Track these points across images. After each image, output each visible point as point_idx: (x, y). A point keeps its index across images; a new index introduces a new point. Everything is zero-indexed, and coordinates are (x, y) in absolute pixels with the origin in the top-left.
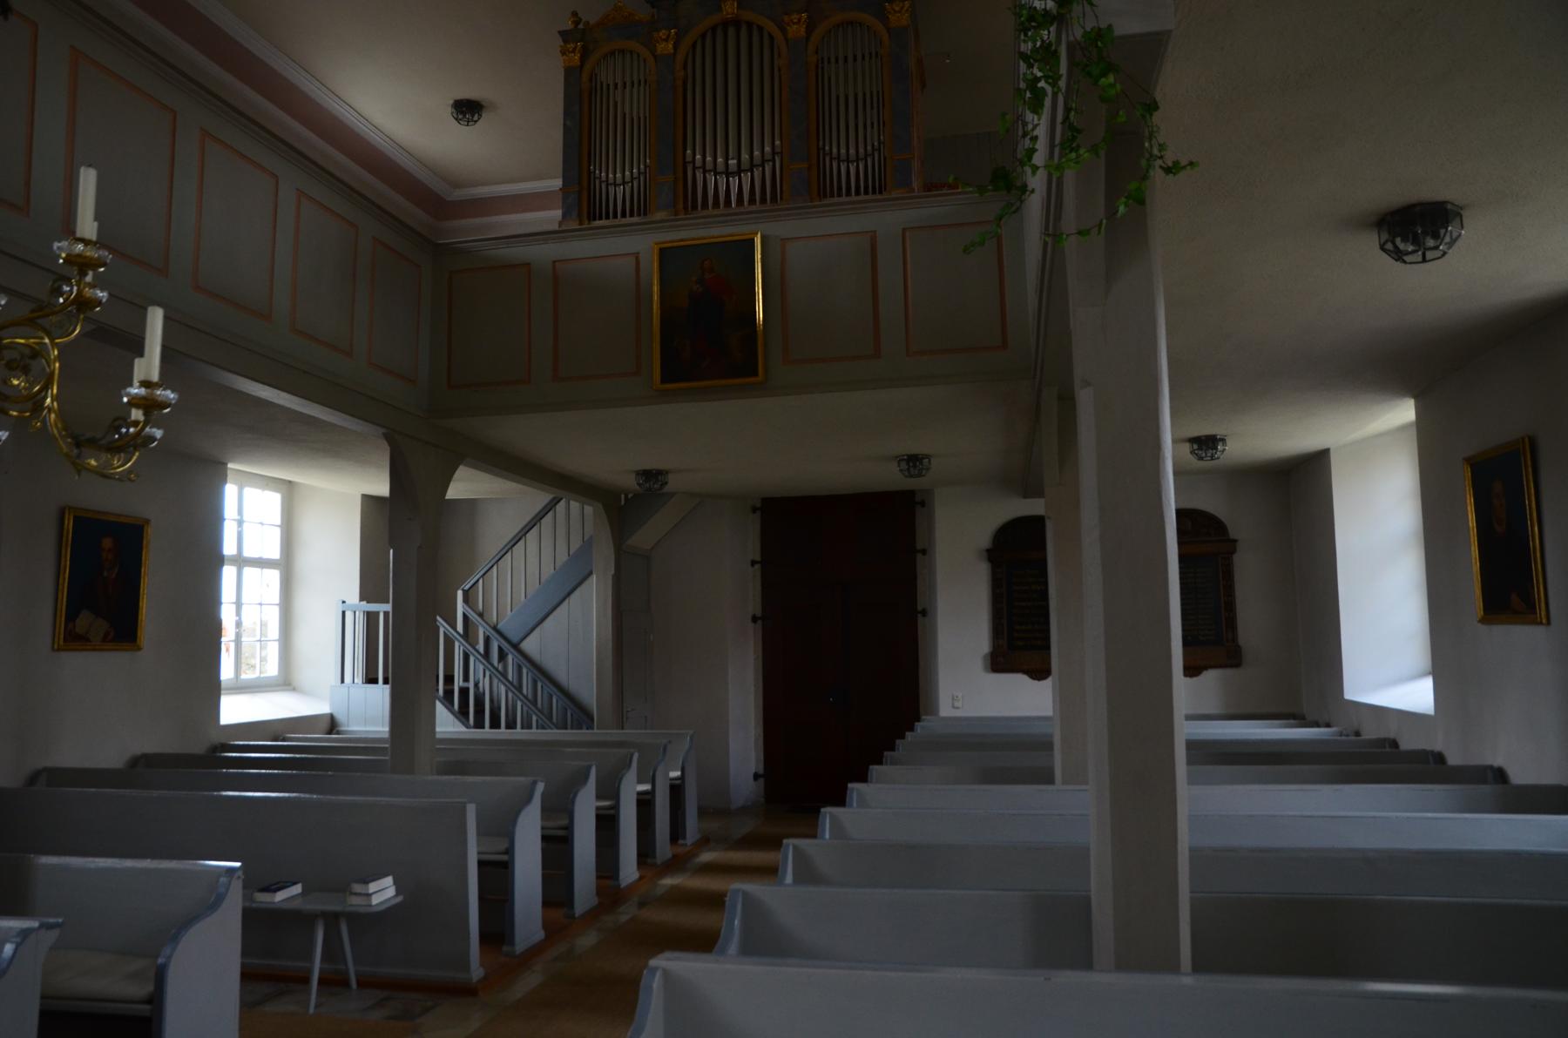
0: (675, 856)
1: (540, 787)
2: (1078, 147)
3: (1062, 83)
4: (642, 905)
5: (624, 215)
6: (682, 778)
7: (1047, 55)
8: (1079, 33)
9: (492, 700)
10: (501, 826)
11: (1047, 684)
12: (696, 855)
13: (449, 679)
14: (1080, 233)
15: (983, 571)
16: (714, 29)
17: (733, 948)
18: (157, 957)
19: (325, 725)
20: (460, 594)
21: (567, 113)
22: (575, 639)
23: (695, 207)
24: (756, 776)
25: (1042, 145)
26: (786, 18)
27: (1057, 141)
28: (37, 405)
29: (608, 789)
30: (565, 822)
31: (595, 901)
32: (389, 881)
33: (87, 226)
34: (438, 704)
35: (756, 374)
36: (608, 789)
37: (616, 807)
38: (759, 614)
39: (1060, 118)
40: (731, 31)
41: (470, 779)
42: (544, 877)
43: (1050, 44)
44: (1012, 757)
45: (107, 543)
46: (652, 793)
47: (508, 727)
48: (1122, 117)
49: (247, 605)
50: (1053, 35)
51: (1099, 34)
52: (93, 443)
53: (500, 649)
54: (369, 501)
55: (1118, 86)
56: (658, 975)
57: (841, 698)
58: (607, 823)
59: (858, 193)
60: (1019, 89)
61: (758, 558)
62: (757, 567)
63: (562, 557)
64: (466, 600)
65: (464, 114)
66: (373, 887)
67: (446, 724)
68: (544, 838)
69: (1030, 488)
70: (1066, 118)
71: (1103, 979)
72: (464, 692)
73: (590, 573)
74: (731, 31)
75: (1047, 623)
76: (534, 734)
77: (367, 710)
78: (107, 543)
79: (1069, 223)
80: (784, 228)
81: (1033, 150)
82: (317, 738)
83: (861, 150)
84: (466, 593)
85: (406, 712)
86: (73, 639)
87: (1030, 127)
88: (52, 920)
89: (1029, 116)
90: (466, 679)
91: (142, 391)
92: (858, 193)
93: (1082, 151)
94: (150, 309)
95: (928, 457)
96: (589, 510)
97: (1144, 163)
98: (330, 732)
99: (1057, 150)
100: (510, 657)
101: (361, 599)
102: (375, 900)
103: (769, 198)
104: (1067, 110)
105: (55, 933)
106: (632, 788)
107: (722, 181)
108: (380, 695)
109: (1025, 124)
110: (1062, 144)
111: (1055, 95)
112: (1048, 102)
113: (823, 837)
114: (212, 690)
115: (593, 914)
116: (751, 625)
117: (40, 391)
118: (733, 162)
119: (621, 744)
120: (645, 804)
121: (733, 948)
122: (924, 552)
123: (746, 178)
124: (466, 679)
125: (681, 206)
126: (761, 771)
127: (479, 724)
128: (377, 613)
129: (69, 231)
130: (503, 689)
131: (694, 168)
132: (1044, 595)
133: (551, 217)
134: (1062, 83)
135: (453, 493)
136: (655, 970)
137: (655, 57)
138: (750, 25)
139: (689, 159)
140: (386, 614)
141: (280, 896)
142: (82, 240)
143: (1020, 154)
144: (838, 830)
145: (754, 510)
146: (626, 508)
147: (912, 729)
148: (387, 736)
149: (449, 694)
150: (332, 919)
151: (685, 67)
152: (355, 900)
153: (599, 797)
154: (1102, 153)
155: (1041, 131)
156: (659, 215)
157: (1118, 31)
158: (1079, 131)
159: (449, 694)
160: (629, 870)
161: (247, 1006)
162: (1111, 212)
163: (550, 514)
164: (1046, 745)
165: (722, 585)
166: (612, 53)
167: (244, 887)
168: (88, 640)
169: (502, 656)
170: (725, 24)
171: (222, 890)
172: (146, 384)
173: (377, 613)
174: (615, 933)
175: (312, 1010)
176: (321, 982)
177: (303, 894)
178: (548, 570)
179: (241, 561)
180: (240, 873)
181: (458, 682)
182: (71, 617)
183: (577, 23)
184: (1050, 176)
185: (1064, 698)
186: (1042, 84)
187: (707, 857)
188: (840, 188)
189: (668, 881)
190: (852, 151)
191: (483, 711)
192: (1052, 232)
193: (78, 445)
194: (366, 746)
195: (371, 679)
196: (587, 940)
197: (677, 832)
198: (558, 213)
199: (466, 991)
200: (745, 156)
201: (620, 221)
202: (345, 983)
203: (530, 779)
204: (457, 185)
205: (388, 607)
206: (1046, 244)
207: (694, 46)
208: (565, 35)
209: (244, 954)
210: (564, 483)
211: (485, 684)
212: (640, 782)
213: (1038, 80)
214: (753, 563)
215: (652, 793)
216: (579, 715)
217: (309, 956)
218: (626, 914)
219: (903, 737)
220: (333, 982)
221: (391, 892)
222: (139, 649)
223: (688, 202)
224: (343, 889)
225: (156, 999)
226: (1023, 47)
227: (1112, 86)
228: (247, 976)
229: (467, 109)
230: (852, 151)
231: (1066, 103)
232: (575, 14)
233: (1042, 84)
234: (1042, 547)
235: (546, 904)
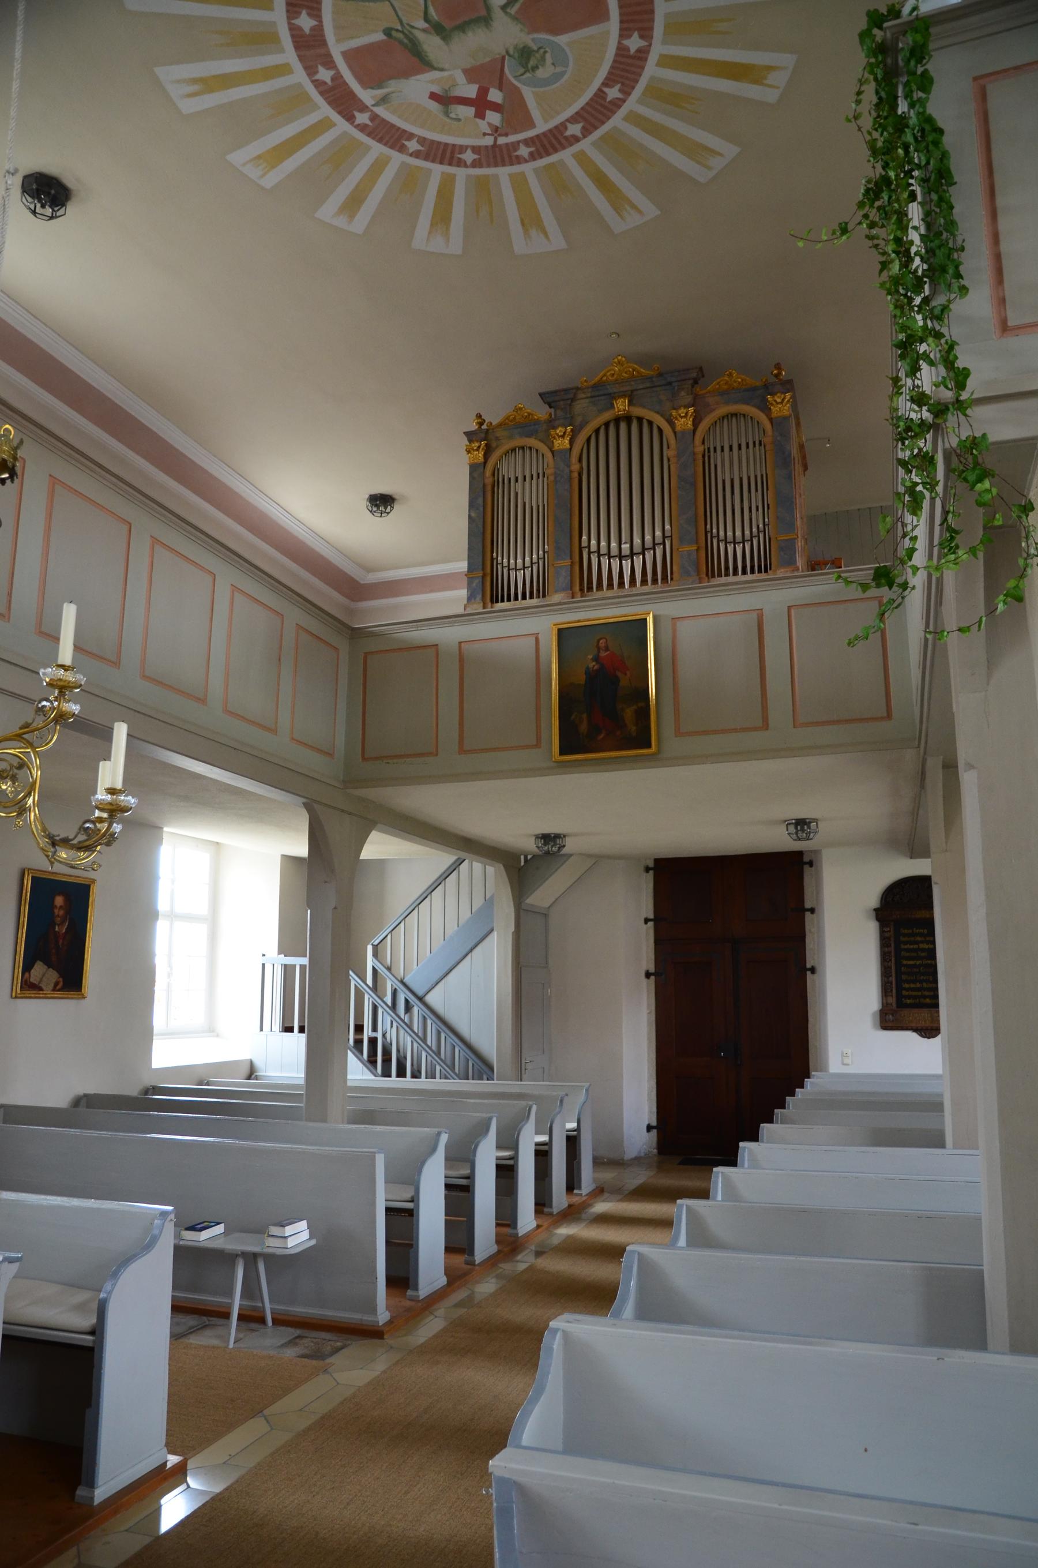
0: (570, 1206)
1: (444, 1138)
2: (957, 547)
3: (940, 488)
4: (539, 1254)
5: (524, 598)
6: (578, 1129)
7: (926, 461)
8: (954, 444)
9: (398, 1051)
10: (407, 1175)
11: (937, 1041)
12: (590, 1205)
13: (359, 1029)
14: (959, 630)
15: (872, 929)
16: (607, 425)
17: (629, 1310)
18: (100, 1291)
19: (245, 1071)
20: (370, 948)
21: (472, 505)
22: (476, 994)
23: (590, 588)
24: (649, 1128)
25: (921, 545)
26: (674, 413)
27: (936, 542)
28: (22, 810)
29: (509, 1141)
30: (466, 1172)
31: (494, 1249)
32: (303, 1225)
33: (66, 653)
34: (349, 1052)
35: (649, 746)
36: (509, 1141)
37: (515, 1158)
38: (652, 970)
39: (938, 520)
40: (623, 426)
41: (379, 1128)
42: (448, 1224)
43: (927, 452)
44: (903, 1120)
45: (59, 901)
46: (549, 1144)
47: (413, 1076)
48: (999, 521)
49: (176, 954)
50: (929, 444)
51: (974, 443)
52: (65, 842)
53: (407, 1001)
54: (290, 862)
55: (994, 491)
56: (559, 1335)
57: (730, 1057)
58: (506, 1172)
59: (744, 572)
60: (898, 494)
61: (652, 916)
62: (651, 924)
63: (466, 915)
64: (375, 955)
65: (377, 506)
66: (289, 1230)
67: (357, 1072)
68: (448, 1187)
69: (917, 849)
70: (945, 520)
71: (997, 1361)
72: (373, 1041)
73: (492, 930)
74: (623, 426)
75: (935, 981)
76: (437, 1084)
77: (284, 1059)
78: (59, 901)
79: (951, 618)
80: (673, 607)
81: (911, 551)
82: (237, 1082)
83: (747, 533)
84: (375, 948)
85: (320, 1062)
86: (29, 988)
87: (909, 528)
88: (13, 1255)
89: (909, 518)
90: (375, 1029)
91: (109, 798)
92: (744, 572)
93: (960, 552)
94: (116, 725)
95: (816, 820)
96: (490, 870)
97: (1021, 562)
98: (249, 1078)
99: (936, 550)
100: (415, 1010)
101: (279, 953)
102: (291, 1243)
103: (661, 576)
104: (945, 513)
105: (15, 1266)
106: (530, 1139)
107: (615, 563)
108: (297, 1042)
109: (904, 525)
110: (940, 544)
111: (933, 499)
112: (926, 504)
113: (715, 1199)
114: (145, 1035)
115: (492, 1261)
116: (644, 981)
117: (25, 797)
118: (626, 547)
119: (520, 1096)
120: (543, 1154)
121: (629, 1310)
122: (812, 911)
123: (638, 561)
124: (375, 1029)
125: (577, 588)
126: (654, 1123)
127: (386, 1073)
128: (294, 966)
129: (52, 659)
130: (409, 1039)
131: (590, 553)
132: (932, 954)
133: (456, 599)
134: (940, 488)
135: (364, 855)
136: (556, 1331)
137: (553, 452)
138: (640, 420)
139: (584, 544)
140: (303, 967)
141: (205, 1235)
142: (62, 666)
143: (902, 553)
144: (731, 1192)
145: (647, 869)
146: (524, 869)
147: (802, 1086)
148: (302, 1082)
149: (358, 1043)
150: (251, 1259)
151: (580, 460)
152: (271, 1242)
153: (499, 1147)
154: (981, 555)
155: (921, 532)
156: (557, 598)
157: (992, 438)
158: (957, 532)
159: (358, 1043)
160: (527, 1219)
161: (176, 1337)
162: (991, 611)
163: (454, 874)
164: (935, 1106)
165: (617, 941)
166: (513, 450)
167: (176, 1225)
168: (42, 990)
169: (408, 1008)
170: (617, 420)
171: (156, 1232)
172: (112, 791)
173: (294, 966)
174: (512, 1283)
175: (231, 1345)
176: (241, 1318)
177: (226, 1233)
178: (452, 928)
179: (172, 916)
180: (172, 1216)
181: (368, 1032)
182: (27, 967)
183: (481, 424)
184: (930, 576)
185: (954, 1057)
186: (920, 488)
187: (601, 1207)
188: (727, 568)
189: (564, 1231)
190: (738, 533)
191: (390, 1060)
192: (934, 630)
193: (54, 844)
194: (282, 1093)
195: (289, 1029)
196: (486, 1287)
197: (572, 1184)
198: (464, 593)
199: (373, 1333)
200: (637, 541)
201: (521, 603)
202: (262, 1320)
203: (436, 1130)
204: (369, 570)
205: (305, 961)
206: (926, 640)
207: (588, 440)
208: (470, 435)
209: (175, 1287)
210: (469, 846)
211: (392, 1035)
212: (538, 1132)
213: (917, 484)
214: (646, 921)
215: (549, 1144)
216: (481, 1066)
217: (230, 1293)
218: (524, 1262)
219: (793, 1094)
220: (251, 1318)
221: (305, 1235)
222: (84, 998)
223: (584, 583)
224: (261, 1230)
225: (97, 1331)
226: (900, 455)
227: (988, 491)
228: (178, 1308)
229: (381, 502)
230: (738, 533)
231: (943, 507)
232: (479, 416)
233: (920, 488)
234: (930, 906)
235: (448, 1250)
